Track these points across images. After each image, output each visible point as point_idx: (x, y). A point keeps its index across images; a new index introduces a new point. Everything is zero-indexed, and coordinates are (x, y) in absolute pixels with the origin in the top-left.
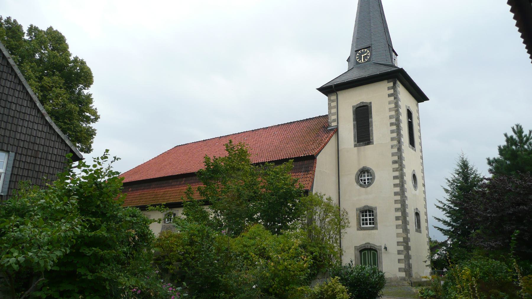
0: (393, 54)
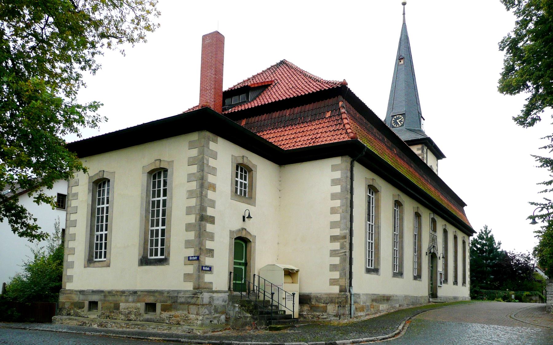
0: (422, 119)
